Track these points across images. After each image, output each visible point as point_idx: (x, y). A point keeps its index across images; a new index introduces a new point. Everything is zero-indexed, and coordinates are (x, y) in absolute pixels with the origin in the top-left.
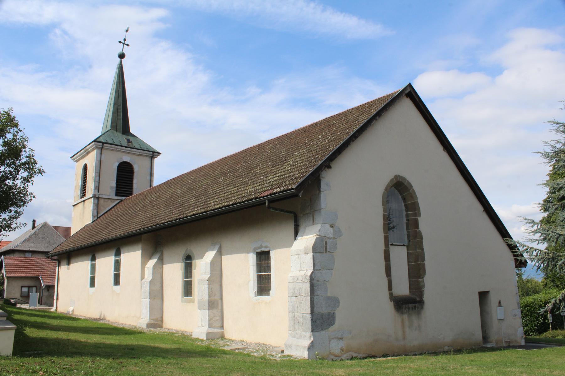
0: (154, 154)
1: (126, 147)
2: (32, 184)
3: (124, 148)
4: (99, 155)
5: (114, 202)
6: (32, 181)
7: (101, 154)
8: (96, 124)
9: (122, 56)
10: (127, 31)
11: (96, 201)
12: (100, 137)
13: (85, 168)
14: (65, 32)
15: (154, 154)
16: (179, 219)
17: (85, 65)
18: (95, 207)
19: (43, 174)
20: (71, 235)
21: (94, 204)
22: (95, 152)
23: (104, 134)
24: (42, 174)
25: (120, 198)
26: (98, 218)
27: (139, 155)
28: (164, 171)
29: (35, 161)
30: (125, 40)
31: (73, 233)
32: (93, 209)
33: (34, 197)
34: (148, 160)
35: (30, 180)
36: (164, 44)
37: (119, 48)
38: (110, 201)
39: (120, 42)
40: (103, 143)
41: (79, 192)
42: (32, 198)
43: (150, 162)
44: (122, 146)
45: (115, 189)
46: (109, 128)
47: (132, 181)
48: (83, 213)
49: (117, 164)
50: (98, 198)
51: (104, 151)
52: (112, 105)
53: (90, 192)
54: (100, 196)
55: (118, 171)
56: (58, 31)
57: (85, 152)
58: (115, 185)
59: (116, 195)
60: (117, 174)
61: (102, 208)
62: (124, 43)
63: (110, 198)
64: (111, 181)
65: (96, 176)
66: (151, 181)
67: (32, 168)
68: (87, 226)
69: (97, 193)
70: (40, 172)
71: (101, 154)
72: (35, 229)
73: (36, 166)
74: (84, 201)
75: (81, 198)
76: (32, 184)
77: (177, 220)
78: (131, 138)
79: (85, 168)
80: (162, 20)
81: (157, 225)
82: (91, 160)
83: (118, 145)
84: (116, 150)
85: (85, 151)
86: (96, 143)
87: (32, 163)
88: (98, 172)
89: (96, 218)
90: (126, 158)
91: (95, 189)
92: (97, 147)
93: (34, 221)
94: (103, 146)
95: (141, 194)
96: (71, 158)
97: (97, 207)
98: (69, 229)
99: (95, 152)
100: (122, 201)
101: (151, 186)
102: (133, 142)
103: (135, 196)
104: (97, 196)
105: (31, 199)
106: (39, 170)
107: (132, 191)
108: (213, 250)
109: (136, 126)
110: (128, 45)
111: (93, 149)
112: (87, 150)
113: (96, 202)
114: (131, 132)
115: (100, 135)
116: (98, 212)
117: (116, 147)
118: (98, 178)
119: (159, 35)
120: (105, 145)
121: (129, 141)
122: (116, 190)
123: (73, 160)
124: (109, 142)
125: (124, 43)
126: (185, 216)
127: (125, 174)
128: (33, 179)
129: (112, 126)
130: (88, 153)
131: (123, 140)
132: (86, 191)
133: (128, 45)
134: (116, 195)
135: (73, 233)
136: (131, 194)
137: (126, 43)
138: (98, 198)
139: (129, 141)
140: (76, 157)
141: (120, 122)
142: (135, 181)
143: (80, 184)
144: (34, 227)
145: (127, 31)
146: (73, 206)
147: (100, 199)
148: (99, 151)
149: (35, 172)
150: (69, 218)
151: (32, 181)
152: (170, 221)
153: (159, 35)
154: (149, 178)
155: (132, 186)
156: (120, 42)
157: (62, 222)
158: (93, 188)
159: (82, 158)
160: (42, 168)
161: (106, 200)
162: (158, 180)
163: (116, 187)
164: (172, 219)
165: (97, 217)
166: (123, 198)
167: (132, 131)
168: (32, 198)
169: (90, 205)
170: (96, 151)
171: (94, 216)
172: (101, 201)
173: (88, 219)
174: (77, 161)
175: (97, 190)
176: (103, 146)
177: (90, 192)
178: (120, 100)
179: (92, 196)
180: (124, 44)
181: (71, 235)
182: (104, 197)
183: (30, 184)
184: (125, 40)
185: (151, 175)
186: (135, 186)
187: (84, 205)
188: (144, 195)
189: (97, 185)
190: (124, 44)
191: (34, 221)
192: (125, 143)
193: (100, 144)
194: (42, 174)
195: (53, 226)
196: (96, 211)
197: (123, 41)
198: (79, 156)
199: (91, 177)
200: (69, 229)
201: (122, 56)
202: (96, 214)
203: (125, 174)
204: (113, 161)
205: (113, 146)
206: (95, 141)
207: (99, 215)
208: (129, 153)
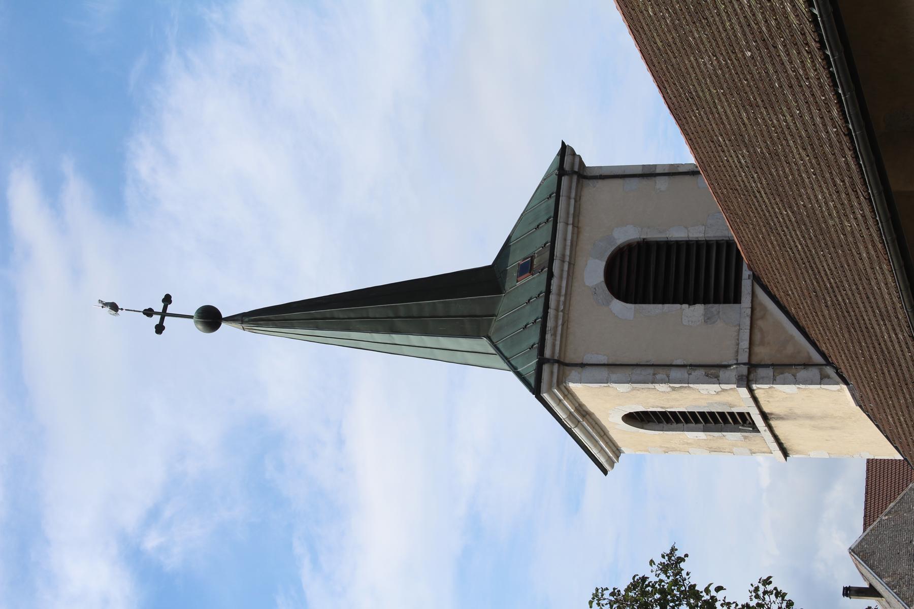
0: (568, 169)
1: (550, 275)
2: (719, 589)
3: (555, 282)
4: (588, 372)
5: (765, 309)
6: (707, 590)
7: (583, 365)
8: (473, 396)
9: (210, 318)
10: (114, 307)
11: (761, 372)
12: (519, 375)
13: (637, 419)
14: (153, 516)
15: (568, 169)
16: (822, 47)
17: (260, 447)
18: (787, 375)
19: (679, 554)
20: (899, 457)
21: (774, 381)
22: (576, 387)
23: (507, 360)
24: (681, 560)
25: (746, 284)
26: (829, 363)
27: (576, 226)
28: (633, 126)
29: (633, 586)
30: (149, 313)
31: (889, 452)
32: (796, 382)
33: (767, 582)
34: (594, 193)
35: (706, 597)
36: (144, 163)
37: (184, 331)
38: (760, 323)
39: (160, 329)
40: (542, 361)
41: (732, 437)
42: (769, 588)
43: (600, 183)
44: (548, 291)
45: (715, 308)
46: (482, 344)
47: (678, 244)
48: (811, 417)
49: (617, 305)
50: (752, 366)
51: (571, 357)
52: (397, 338)
53: (735, 399)
54: (744, 358)
55: (644, 301)
56: (152, 542)
57: (581, 423)
58: (699, 308)
59: (737, 300)
60: (655, 302)
61: (790, 349)
62: (160, 315)
63: (747, 321)
64: (685, 324)
65: (668, 381)
66: (674, 173)
67: (662, 591)
68: (861, 403)
69: (732, 373)
70: (673, 563)
71: (583, 365)
72: (880, 588)
73: (653, 578)
74: (765, 417)
75: (755, 429)
76: (719, 589)
77: (826, 58)
78: (516, 259)
79: (637, 419)
80: (51, 189)
81: (849, 134)
82: (609, 401)
83: (546, 307)
84: (566, 311)
85: (578, 423)
86: (544, 386)
87: (644, 593)
88: (650, 371)
89: (830, 371)
90: (593, 272)
91: (717, 380)
92: (561, 383)
93: (849, 592)
94: (552, 361)
95: (726, 209)
96: (605, 472)
97: (786, 369)
98: (874, 467)
99: (576, 387)
100: (756, 279)
101: (694, 173)
102: (528, 252)
103: (737, 232)
104: (744, 370)
105: (779, 594)
106: (664, 568)
107: (718, 243)
108: (687, 149)
109: (469, 243)
110: (167, 300)
111: (569, 395)
112: (570, 415)
113: (769, 372)
114: (488, 261)
115: (511, 375)
116: (807, 365)
117: (551, 312)
118: (674, 373)
119: (113, 191)
120: (548, 353)
121: (526, 268)
122: (716, 301)
123: (612, 464)
124: (535, 339)
125: (160, 315)
126: (809, 27)
127: (651, 272)
128: (700, 588)
129: (476, 335)
130: (583, 413)
131: (522, 290)
132: (726, 410)
133: (167, 300)
134: (737, 300)
135: (889, 452)
136: (730, 244)
137: (159, 307)
138: (752, 366)
139: (526, 268)
140: (603, 453)
141: (459, 305)
142: (677, 234)
143: (702, 435)
144: (871, 592)
145: (114, 307)
146: (785, 454)
147: (755, 360)
148: (574, 373)
149: (675, 583)
150: (829, 469)
151: (707, 590)
152: (835, 85)
153: (113, 191)
154: (662, 184)
155: (698, 243)
156: (160, 329)
157: (849, 497)
158: (714, 388)
159: (603, 433)
160: (658, 560)
161: (757, 336)
162: (671, 148)
163: (705, 302)
164: (825, 80)
165: (824, 367)
166: (746, 273)
167: (485, 258)
168: (769, 588)
169: (778, 396)
170: (572, 386)
171: (823, 379)
172: (763, 353)
173: (837, 398)
174: (617, 452)
175: (722, 373)
176: (552, 361)
177: (735, 399)
178: (373, 310)
179: (744, 391)
180: (164, 314)
181: (899, 457)
182: (745, 344)
183: (720, 596)
184: (149, 313)
185: (648, 174)
186: (696, 233)
187: (780, 418)
188: (728, 193)
189: (700, 372)
190: (164, 314)
191: (849, 592)
192: (535, 282)
193: (545, 373)
194: (681, 560)
195: (864, 530)
196: (802, 373)
197: (156, 319)
198: (596, 443)
199: (675, 395)
200: (874, 467)
201: (210, 318)
202: (814, 372)
203: (651, 272)
204: (604, 319)
205: (550, 324)
206: (536, 391)
207: (817, 358)
208: (571, 264)
